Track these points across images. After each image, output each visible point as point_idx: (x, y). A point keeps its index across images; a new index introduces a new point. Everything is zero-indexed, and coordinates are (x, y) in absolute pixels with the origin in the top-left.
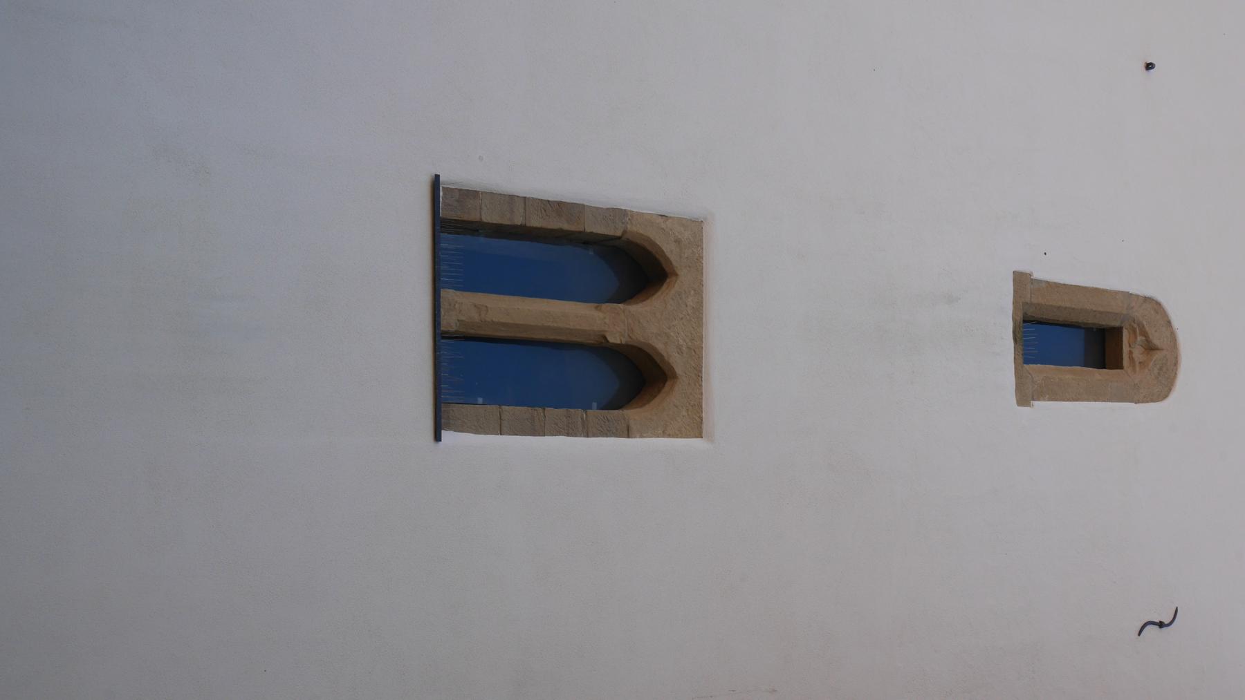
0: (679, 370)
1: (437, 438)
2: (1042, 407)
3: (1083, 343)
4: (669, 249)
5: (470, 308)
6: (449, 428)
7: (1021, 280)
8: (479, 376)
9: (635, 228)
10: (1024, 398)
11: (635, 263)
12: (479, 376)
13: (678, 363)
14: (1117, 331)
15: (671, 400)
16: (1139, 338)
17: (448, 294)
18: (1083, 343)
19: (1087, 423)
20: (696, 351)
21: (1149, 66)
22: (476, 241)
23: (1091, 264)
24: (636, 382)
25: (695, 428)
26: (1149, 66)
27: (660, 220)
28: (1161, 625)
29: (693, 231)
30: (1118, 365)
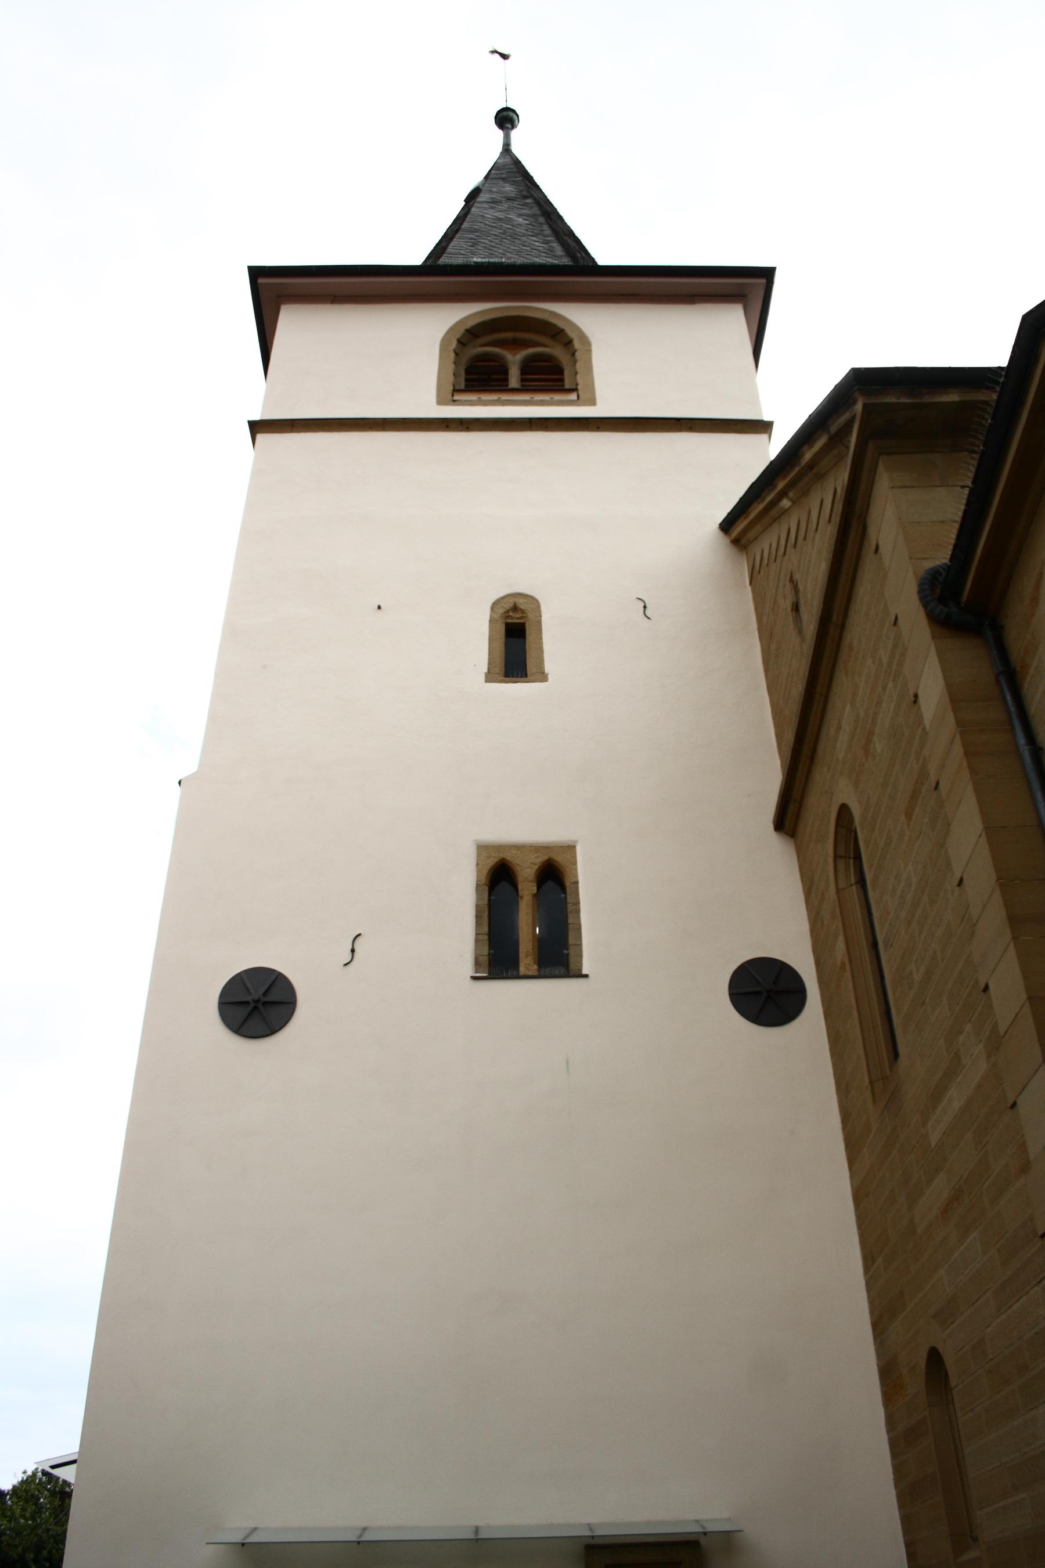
0: (546, 858)
1: (586, 976)
2: (549, 667)
3: (516, 644)
4: (491, 862)
5: (527, 962)
6: (581, 970)
7: (490, 678)
8: (558, 957)
9: (483, 879)
10: (543, 677)
11: (499, 877)
12: (558, 957)
13: (539, 859)
14: (507, 625)
15: (560, 859)
16: (511, 614)
17: (522, 970)
18: (516, 644)
19: (554, 644)
20: (537, 848)
21: (379, 607)
22: (498, 959)
23: (477, 644)
24: (554, 875)
25: (571, 848)
26: (379, 607)
27: (873, 547)
28: (645, 607)
29: (483, 849)
30: (523, 625)
